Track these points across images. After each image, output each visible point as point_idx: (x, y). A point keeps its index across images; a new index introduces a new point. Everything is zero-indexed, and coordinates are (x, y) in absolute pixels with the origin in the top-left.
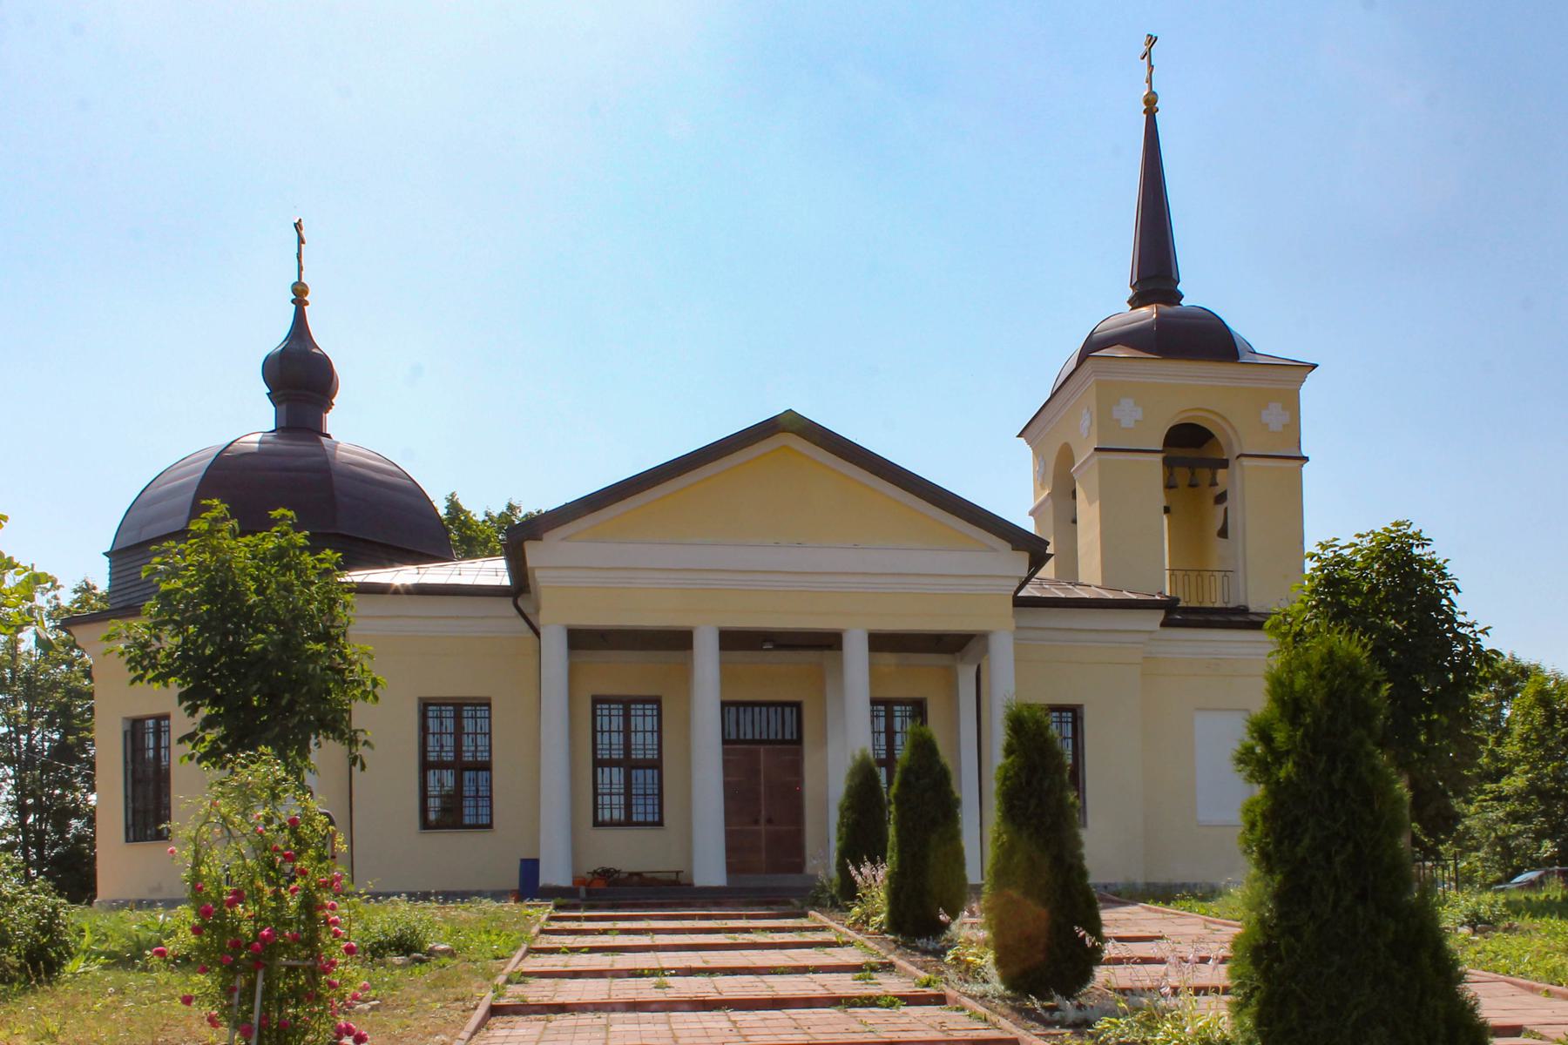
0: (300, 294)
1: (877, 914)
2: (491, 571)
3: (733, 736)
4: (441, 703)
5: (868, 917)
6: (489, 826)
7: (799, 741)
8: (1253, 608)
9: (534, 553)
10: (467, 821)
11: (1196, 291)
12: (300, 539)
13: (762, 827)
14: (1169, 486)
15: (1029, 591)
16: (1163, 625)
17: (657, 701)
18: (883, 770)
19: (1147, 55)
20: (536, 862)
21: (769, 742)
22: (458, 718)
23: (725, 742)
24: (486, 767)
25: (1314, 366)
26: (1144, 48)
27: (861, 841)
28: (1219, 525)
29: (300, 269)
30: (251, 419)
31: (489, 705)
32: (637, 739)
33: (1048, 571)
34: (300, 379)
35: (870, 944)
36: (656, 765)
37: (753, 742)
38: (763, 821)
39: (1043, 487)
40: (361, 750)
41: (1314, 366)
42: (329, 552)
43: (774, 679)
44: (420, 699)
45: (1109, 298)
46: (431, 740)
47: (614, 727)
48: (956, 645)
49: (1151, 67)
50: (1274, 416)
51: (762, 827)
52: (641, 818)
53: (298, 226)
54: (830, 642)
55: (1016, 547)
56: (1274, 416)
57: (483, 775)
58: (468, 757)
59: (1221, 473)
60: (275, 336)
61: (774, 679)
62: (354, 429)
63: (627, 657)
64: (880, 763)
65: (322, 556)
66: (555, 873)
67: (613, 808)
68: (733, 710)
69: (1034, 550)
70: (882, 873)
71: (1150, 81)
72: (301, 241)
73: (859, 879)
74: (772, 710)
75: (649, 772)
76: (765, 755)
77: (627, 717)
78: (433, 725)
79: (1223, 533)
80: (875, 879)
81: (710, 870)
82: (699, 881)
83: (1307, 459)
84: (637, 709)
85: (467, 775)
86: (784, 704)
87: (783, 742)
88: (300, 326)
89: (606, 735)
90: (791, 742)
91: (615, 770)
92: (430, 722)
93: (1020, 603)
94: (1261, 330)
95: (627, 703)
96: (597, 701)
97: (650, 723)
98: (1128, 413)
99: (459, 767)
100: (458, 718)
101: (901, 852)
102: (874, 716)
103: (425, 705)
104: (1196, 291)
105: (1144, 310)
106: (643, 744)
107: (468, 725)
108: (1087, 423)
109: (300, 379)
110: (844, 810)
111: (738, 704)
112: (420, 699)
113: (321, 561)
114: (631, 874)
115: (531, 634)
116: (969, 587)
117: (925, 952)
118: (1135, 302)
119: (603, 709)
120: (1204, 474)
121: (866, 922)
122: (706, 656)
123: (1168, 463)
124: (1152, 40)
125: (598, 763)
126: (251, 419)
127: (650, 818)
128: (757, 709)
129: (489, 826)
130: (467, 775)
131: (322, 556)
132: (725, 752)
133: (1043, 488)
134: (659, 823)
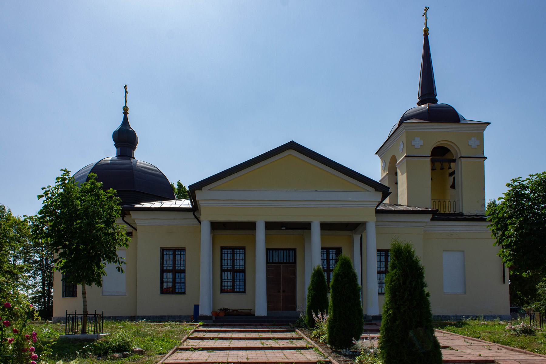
0: (126, 110)
1: (323, 334)
2: (185, 203)
3: (271, 261)
4: (168, 249)
5: (320, 335)
6: (184, 293)
7: (295, 263)
8: (465, 213)
9: (199, 195)
10: (177, 291)
11: (442, 99)
12: (99, 184)
13: (281, 294)
14: (433, 169)
15: (381, 207)
16: (432, 220)
17: (244, 248)
18: (326, 273)
19: (425, 14)
20: (198, 305)
21: (283, 263)
22: (174, 255)
23: (268, 263)
24: (184, 272)
25: (489, 123)
26: (424, 12)
27: (317, 303)
28: (451, 183)
29: (126, 102)
30: (109, 153)
31: (185, 250)
32: (237, 262)
33: (387, 201)
34: (125, 139)
35: (321, 350)
36: (243, 271)
37: (278, 263)
38: (281, 292)
39: (384, 171)
40: (122, 265)
41: (489, 123)
42: (111, 189)
43: (284, 241)
44: (161, 248)
45: (410, 102)
46: (165, 262)
47: (229, 258)
48: (355, 227)
49: (426, 18)
50: (473, 142)
51: (281, 294)
52: (238, 290)
53: (125, 87)
54: (306, 226)
55: (377, 190)
56: (473, 142)
57: (183, 274)
58: (177, 268)
59: (452, 164)
60: (117, 125)
61: (284, 241)
62: (142, 156)
63: (232, 233)
64: (325, 271)
65: (109, 191)
66: (205, 311)
67: (228, 285)
68: (271, 251)
69: (383, 190)
70: (327, 317)
71: (426, 24)
72: (126, 92)
73: (316, 319)
74: (285, 251)
75: (241, 274)
76: (282, 269)
77: (233, 254)
78: (165, 257)
79: (453, 186)
80: (324, 321)
81: (261, 310)
82: (257, 314)
83: (486, 158)
84: (236, 251)
85: (177, 274)
86: (289, 249)
87: (289, 263)
88: (125, 121)
89: (238, 261)
90: (292, 263)
91: (229, 273)
92: (165, 256)
93: (378, 212)
94: (467, 113)
95: (233, 249)
96: (222, 248)
97: (242, 256)
98: (418, 143)
99: (174, 272)
100: (174, 255)
101: (334, 310)
102: (322, 254)
103: (163, 250)
104: (442, 99)
105: (423, 106)
106: (239, 264)
107: (177, 257)
108: (402, 147)
109: (125, 139)
110: (310, 290)
111: (273, 249)
112: (161, 248)
113: (108, 193)
114: (234, 310)
115: (197, 222)
116: (359, 206)
117: (345, 356)
118: (419, 104)
119: (225, 251)
120: (446, 165)
121: (319, 338)
122: (261, 232)
123: (432, 161)
124: (427, 9)
125: (222, 271)
126: (109, 153)
127: (241, 290)
128: (280, 251)
129: (184, 293)
130: (177, 274)
131: (109, 191)
132: (268, 267)
133: (384, 171)
134: (244, 292)
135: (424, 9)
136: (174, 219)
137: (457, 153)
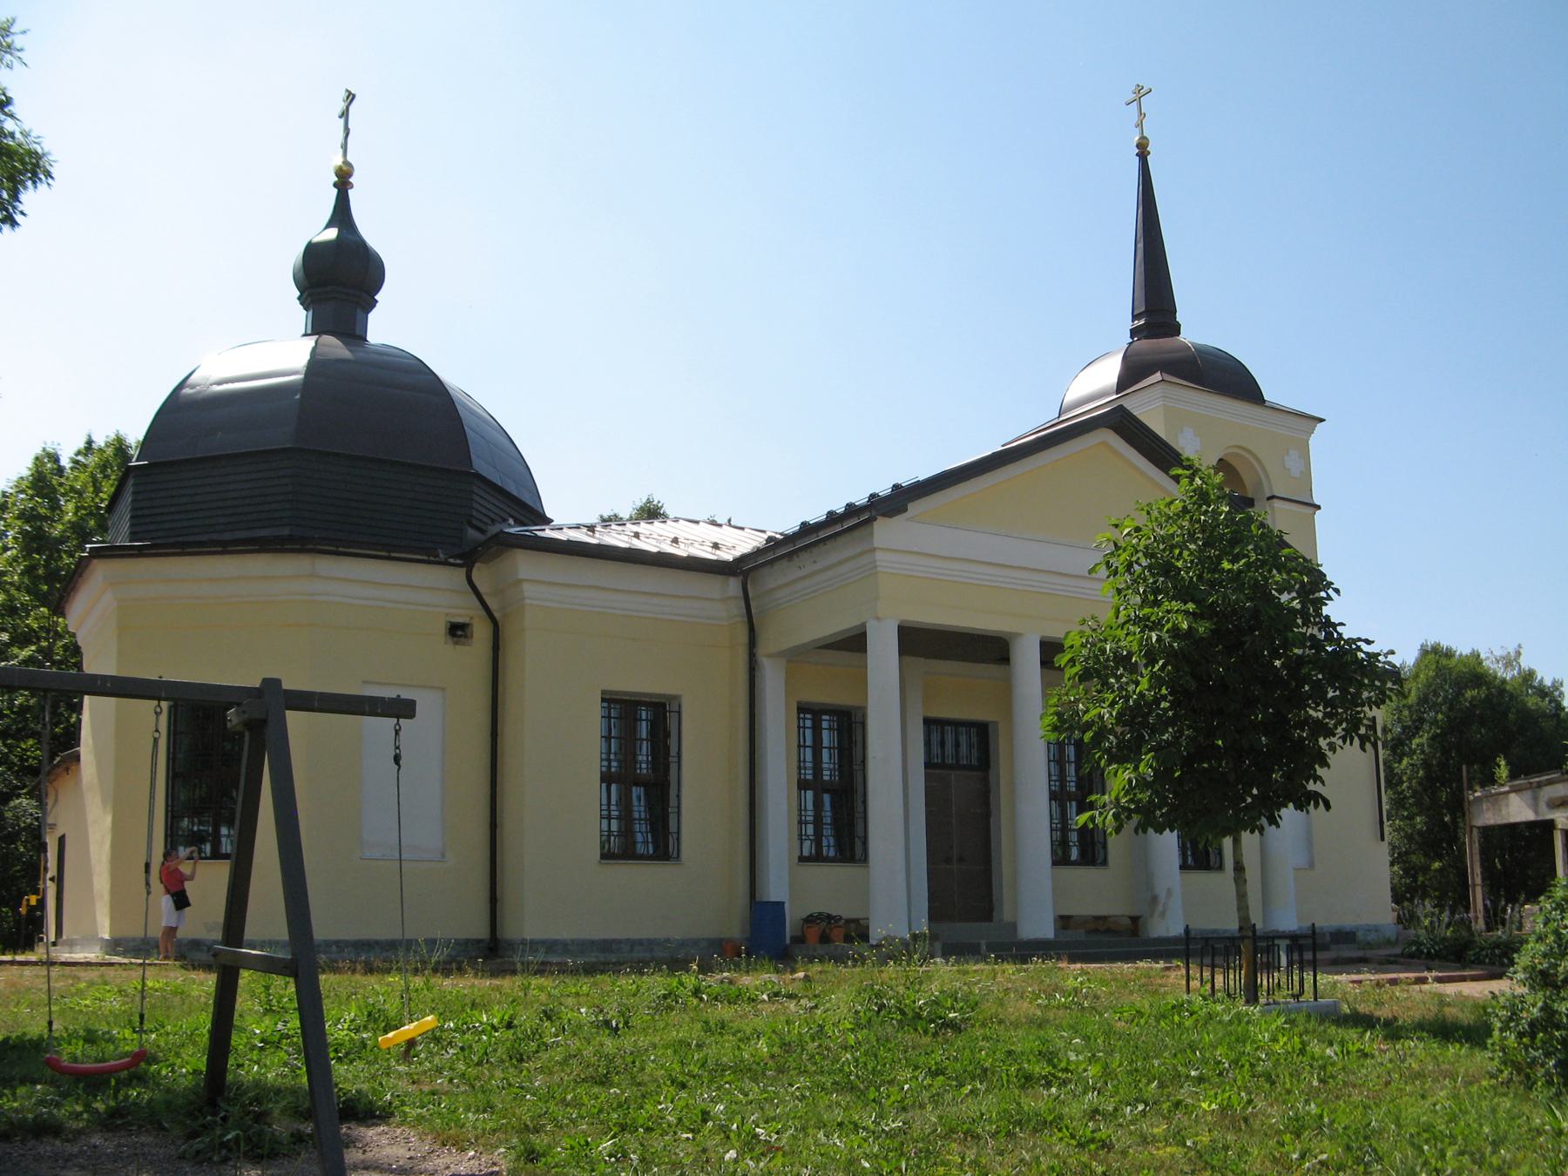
19: (345, 115)
34: (339, 278)
50: (1292, 461)
83: (1319, 507)
86: (969, 724)
109: (339, 278)
112: (610, 700)
124: (351, 97)
135: (344, 95)
136: (657, 594)
137: (1260, 483)
